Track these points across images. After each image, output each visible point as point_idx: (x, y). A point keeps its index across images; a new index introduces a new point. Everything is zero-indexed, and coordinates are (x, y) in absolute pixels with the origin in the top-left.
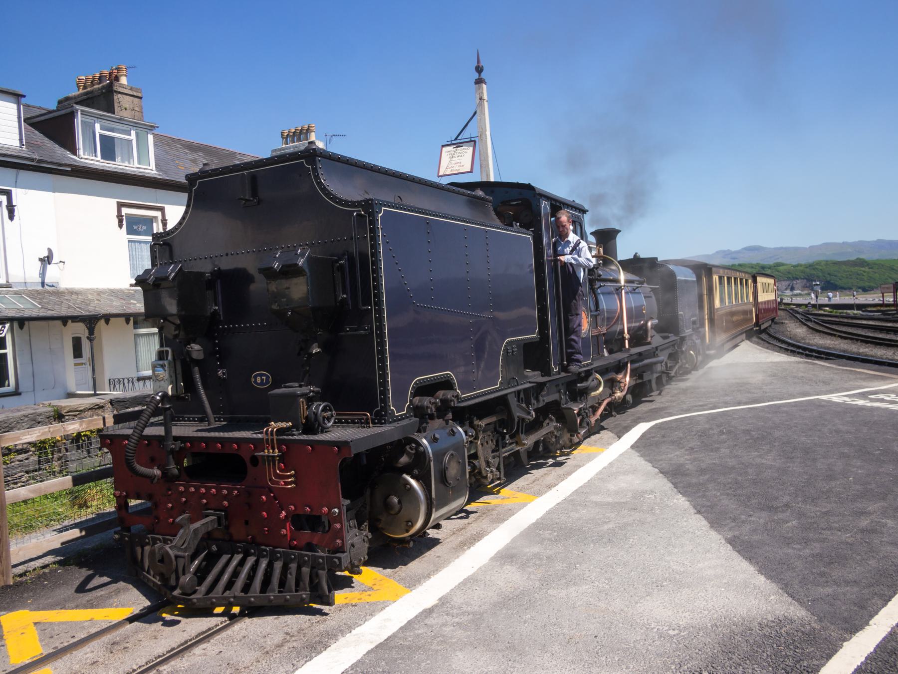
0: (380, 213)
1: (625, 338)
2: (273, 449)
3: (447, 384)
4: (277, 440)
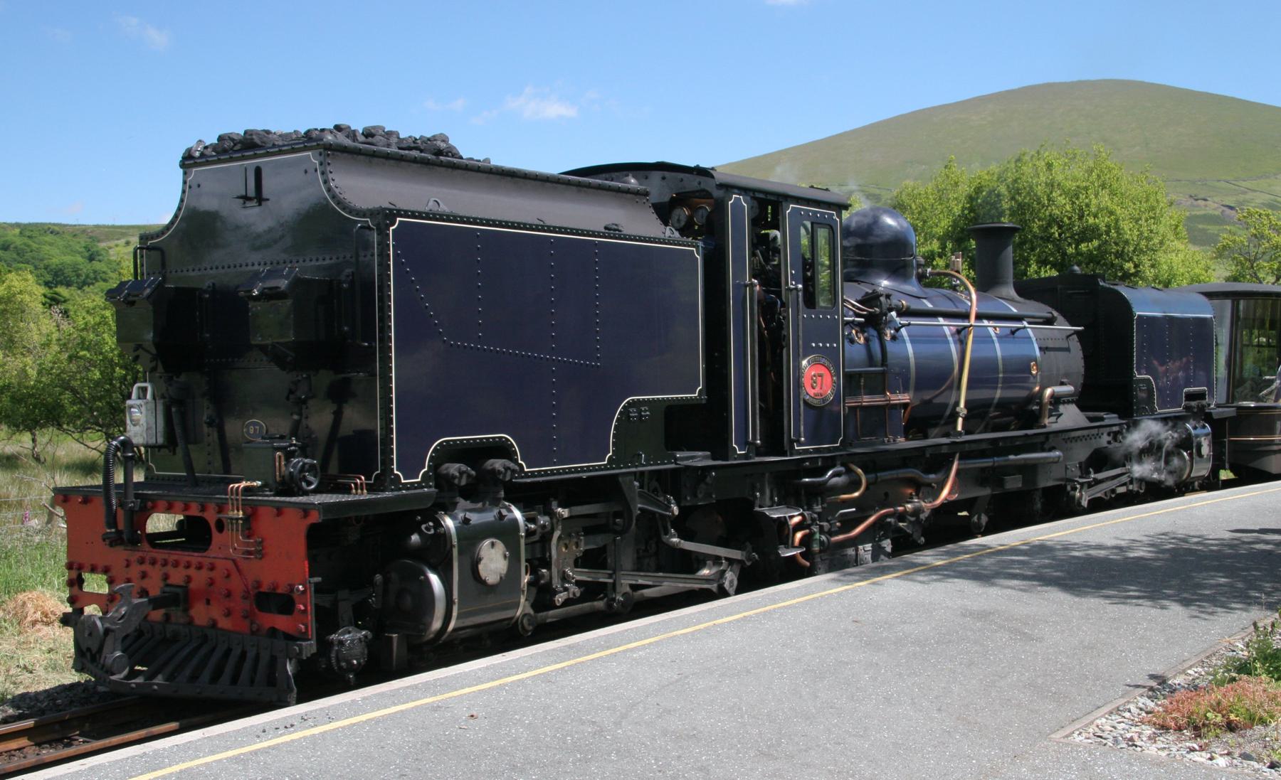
0: (393, 225)
1: (958, 413)
2: (238, 510)
3: (502, 450)
4: (242, 495)
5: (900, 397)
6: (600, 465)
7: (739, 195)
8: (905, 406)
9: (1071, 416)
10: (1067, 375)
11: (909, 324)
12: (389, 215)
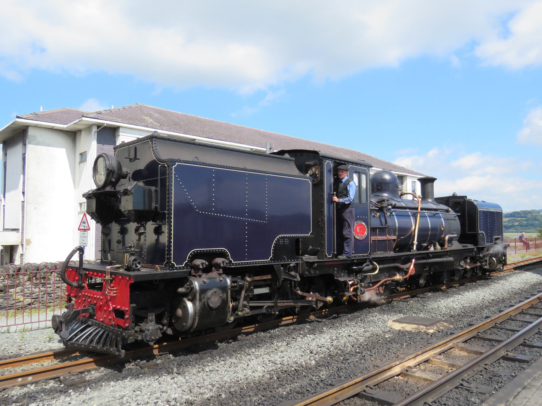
3: (222, 255)
5: (392, 237)
6: (266, 261)
7: (329, 160)
8: (394, 240)
9: (456, 246)
10: (455, 231)
11: (396, 211)
12: (173, 161)
